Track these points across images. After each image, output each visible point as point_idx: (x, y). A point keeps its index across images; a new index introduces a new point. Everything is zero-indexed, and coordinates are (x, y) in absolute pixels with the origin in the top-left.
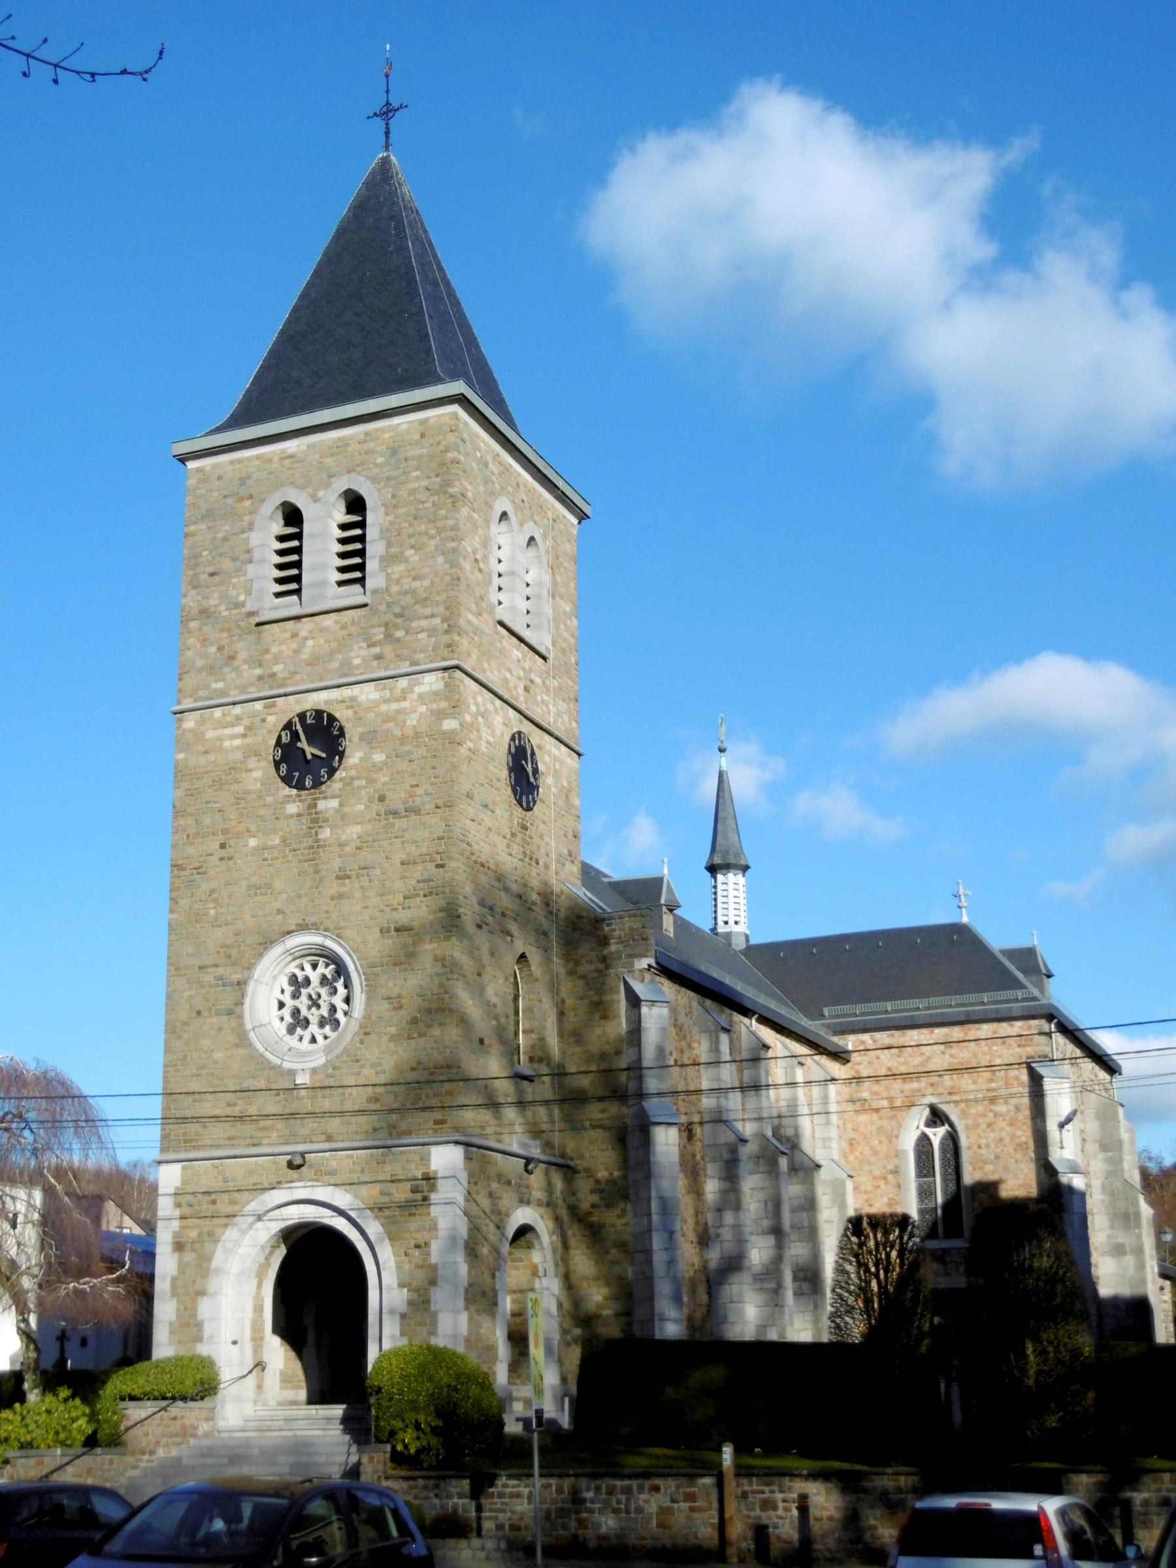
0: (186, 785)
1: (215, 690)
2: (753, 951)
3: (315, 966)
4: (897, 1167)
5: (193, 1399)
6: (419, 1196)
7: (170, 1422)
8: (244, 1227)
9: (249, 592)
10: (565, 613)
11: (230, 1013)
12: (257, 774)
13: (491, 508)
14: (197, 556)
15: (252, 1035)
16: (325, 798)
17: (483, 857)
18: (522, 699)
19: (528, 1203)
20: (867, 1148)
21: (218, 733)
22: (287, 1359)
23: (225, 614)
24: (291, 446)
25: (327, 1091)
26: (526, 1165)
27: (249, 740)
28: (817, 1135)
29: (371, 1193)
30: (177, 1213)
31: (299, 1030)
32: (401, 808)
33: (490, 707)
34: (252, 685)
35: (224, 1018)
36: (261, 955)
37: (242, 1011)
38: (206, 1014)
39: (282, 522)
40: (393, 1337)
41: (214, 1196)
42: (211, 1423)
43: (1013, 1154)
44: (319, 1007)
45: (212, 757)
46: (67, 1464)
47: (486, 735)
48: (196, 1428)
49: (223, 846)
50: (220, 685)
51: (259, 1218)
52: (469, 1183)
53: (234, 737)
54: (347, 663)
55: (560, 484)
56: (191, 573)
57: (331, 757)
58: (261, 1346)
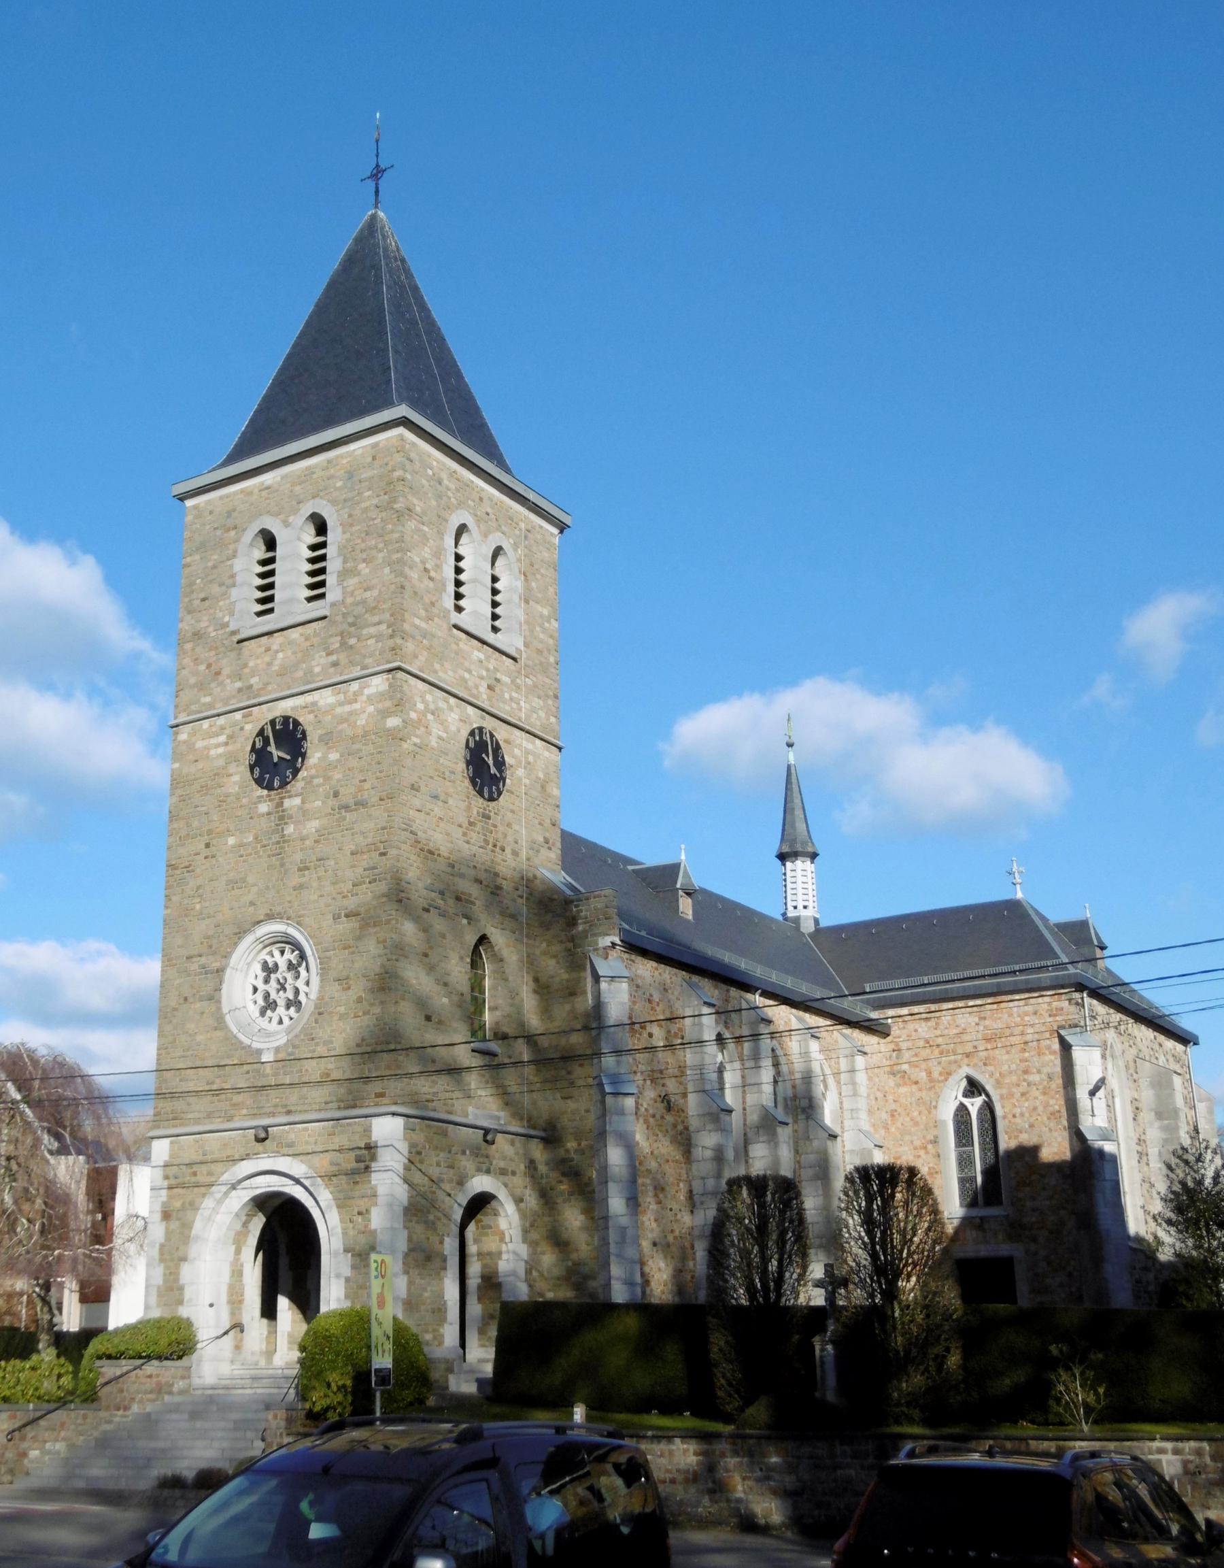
0: (179, 792)
1: (204, 704)
2: (820, 932)
3: (282, 953)
4: (936, 1137)
5: (167, 1359)
6: (362, 1165)
7: (144, 1380)
8: (218, 1196)
9: (232, 614)
10: (542, 616)
11: (210, 998)
12: (236, 778)
13: (446, 521)
14: (192, 584)
15: (228, 1018)
16: (290, 797)
17: (431, 844)
18: (485, 697)
19: (488, 1172)
20: (908, 1119)
21: (205, 743)
22: (294, 1321)
23: (213, 634)
24: (268, 478)
25: (199, 1063)
26: (485, 1135)
27: (230, 748)
28: (846, 1106)
29: (323, 1162)
30: (166, 1183)
31: (269, 1012)
32: (351, 802)
33: (442, 704)
34: (234, 697)
35: (205, 1003)
36: (236, 944)
37: (220, 997)
38: (191, 1000)
39: (264, 548)
40: (338, 1300)
41: (195, 1168)
42: (186, 1381)
43: (1047, 1122)
44: (285, 989)
45: (200, 765)
46: (41, 1417)
47: (436, 730)
48: (172, 1385)
49: (207, 846)
50: (208, 699)
51: (234, 1187)
52: (410, 1152)
53: (217, 746)
54: (310, 671)
55: (531, 496)
56: (187, 600)
57: (294, 759)
58: (240, 1309)
